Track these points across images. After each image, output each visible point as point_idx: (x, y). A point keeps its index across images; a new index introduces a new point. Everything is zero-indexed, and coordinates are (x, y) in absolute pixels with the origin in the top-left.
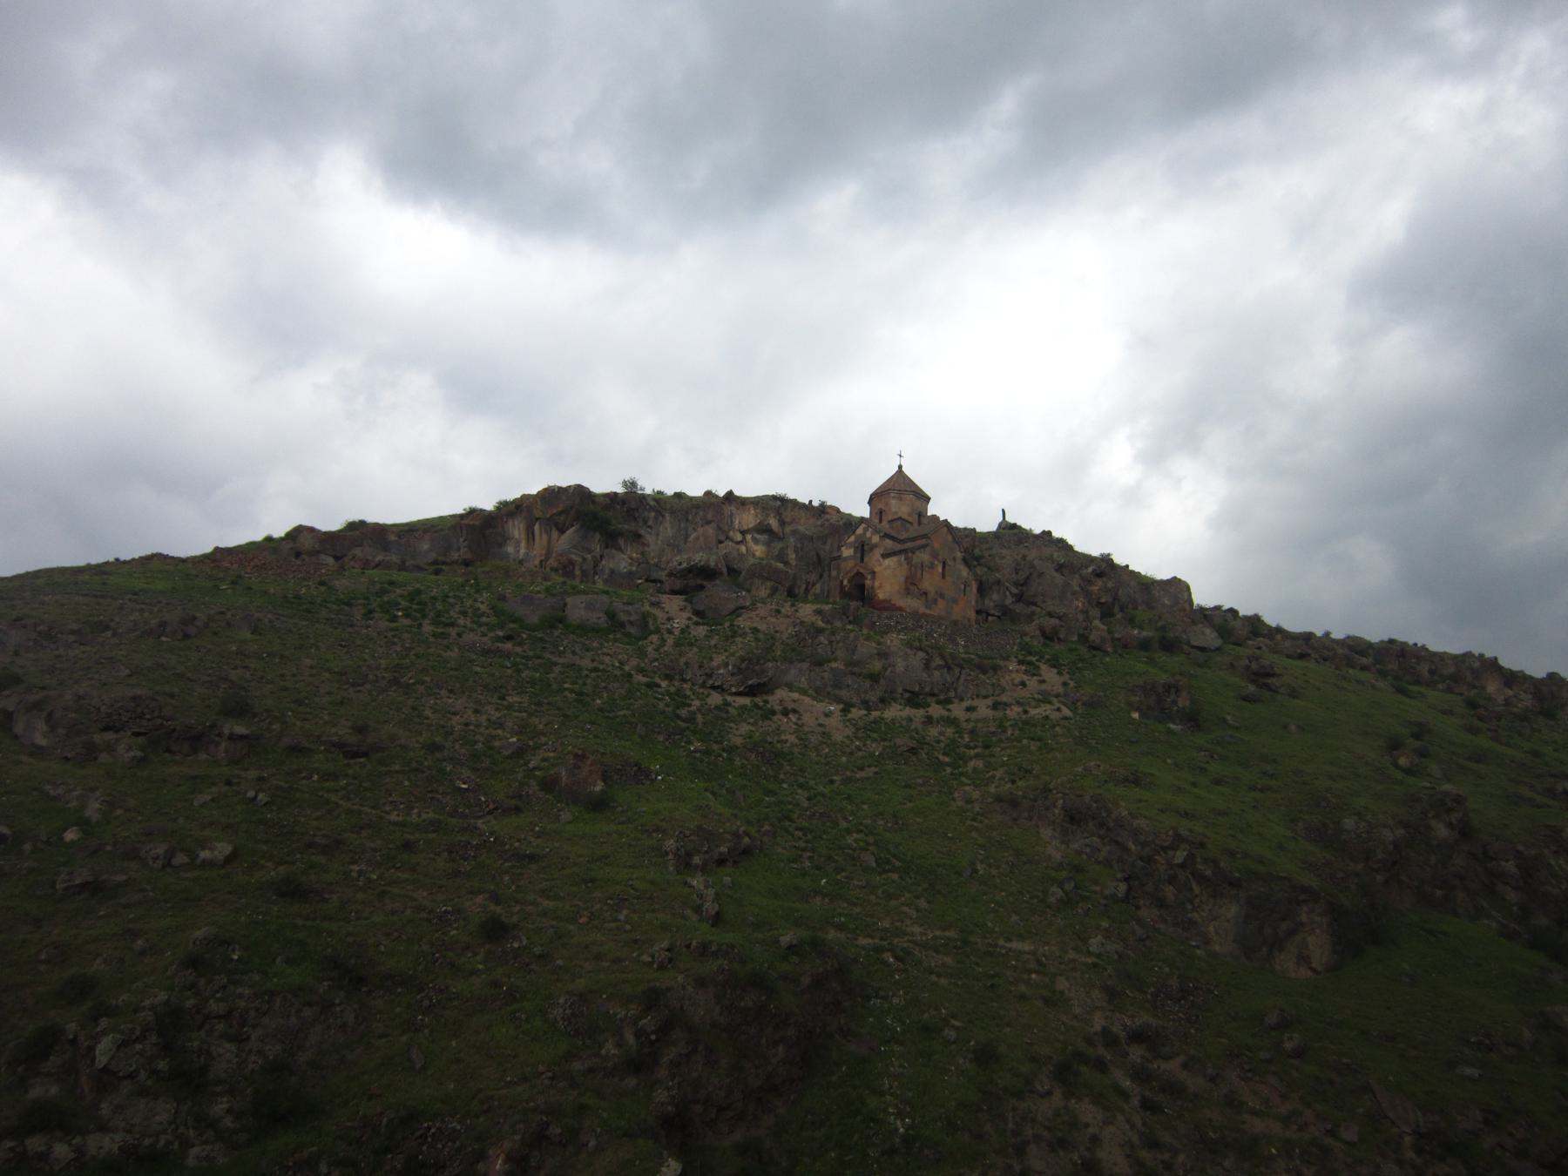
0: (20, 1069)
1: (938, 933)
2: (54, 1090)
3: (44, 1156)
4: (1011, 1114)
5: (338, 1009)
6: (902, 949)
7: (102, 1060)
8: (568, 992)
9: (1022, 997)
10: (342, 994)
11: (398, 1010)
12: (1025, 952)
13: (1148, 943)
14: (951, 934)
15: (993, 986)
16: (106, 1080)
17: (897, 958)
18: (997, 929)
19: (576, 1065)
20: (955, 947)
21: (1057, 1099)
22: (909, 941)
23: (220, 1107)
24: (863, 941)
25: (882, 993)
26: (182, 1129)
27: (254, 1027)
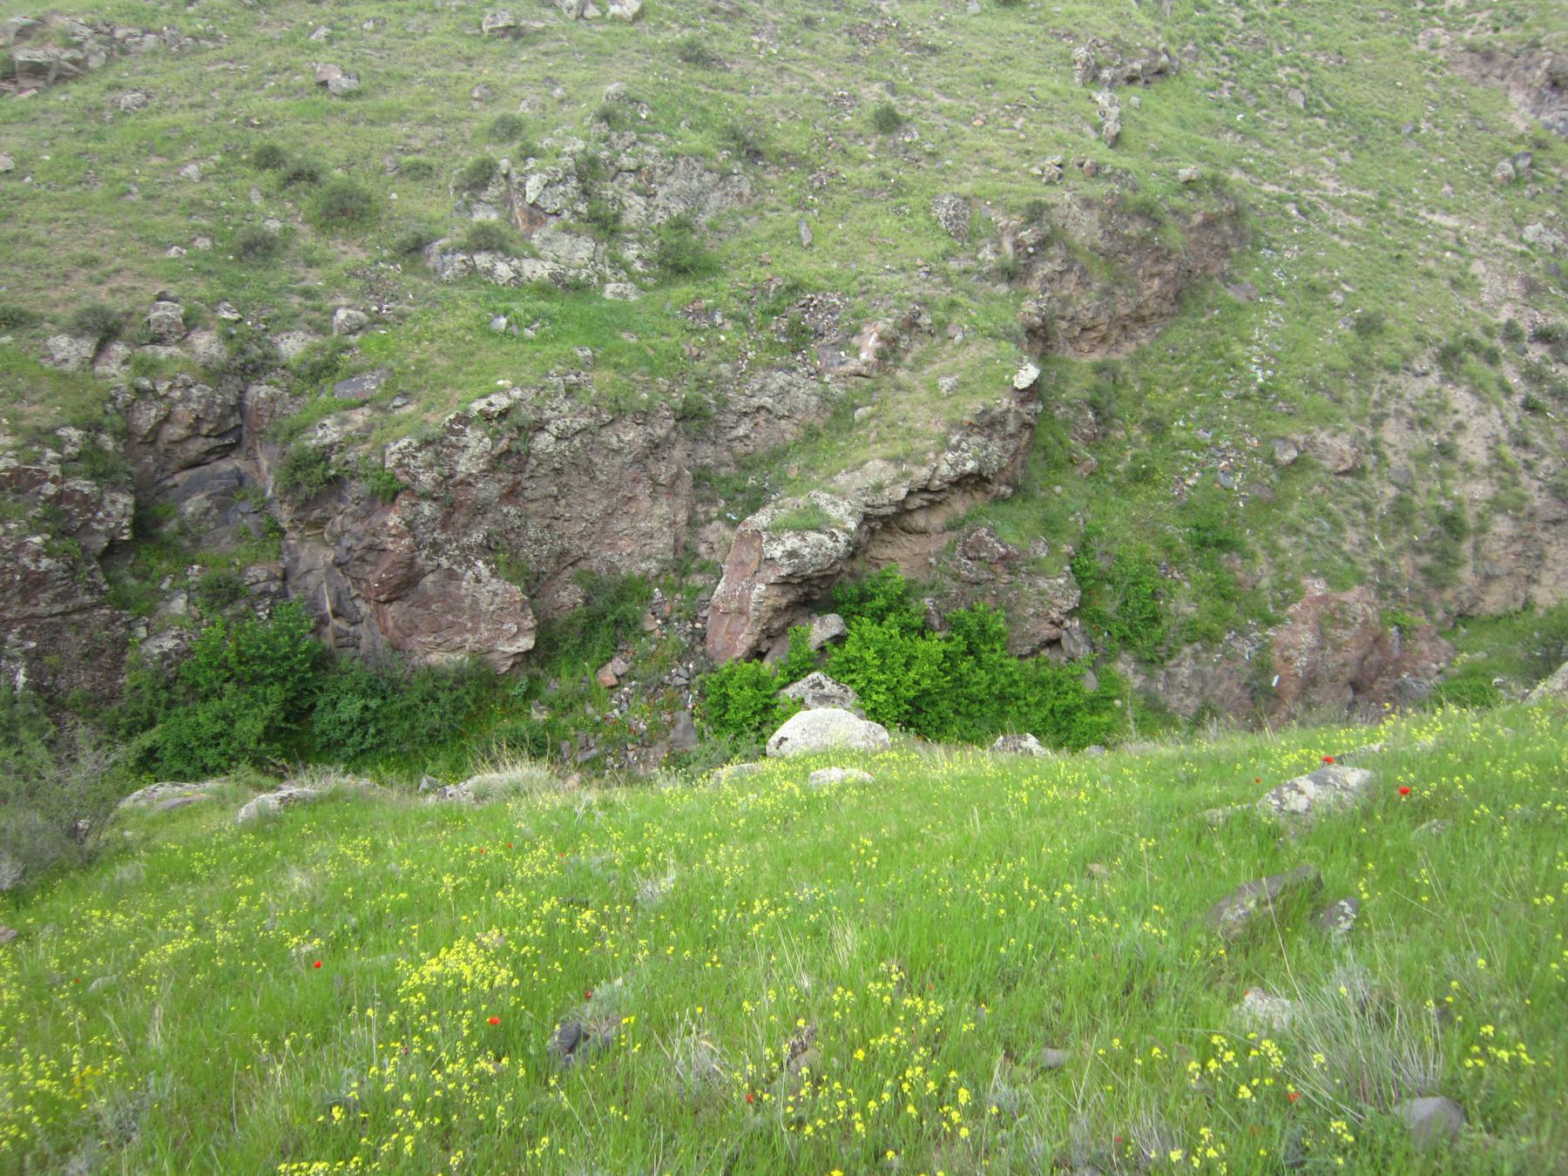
1: (1354, 192)
2: (494, 217)
3: (490, 272)
6: (1309, 203)
9: (1429, 275)
10: (739, 164)
12: (1446, 228)
14: (1369, 195)
15: (1398, 257)
16: (536, 215)
17: (1301, 211)
19: (953, 265)
20: (1369, 210)
21: (1432, 381)
23: (630, 253)
24: (1267, 188)
25: (1275, 245)
26: (600, 266)
27: (661, 184)
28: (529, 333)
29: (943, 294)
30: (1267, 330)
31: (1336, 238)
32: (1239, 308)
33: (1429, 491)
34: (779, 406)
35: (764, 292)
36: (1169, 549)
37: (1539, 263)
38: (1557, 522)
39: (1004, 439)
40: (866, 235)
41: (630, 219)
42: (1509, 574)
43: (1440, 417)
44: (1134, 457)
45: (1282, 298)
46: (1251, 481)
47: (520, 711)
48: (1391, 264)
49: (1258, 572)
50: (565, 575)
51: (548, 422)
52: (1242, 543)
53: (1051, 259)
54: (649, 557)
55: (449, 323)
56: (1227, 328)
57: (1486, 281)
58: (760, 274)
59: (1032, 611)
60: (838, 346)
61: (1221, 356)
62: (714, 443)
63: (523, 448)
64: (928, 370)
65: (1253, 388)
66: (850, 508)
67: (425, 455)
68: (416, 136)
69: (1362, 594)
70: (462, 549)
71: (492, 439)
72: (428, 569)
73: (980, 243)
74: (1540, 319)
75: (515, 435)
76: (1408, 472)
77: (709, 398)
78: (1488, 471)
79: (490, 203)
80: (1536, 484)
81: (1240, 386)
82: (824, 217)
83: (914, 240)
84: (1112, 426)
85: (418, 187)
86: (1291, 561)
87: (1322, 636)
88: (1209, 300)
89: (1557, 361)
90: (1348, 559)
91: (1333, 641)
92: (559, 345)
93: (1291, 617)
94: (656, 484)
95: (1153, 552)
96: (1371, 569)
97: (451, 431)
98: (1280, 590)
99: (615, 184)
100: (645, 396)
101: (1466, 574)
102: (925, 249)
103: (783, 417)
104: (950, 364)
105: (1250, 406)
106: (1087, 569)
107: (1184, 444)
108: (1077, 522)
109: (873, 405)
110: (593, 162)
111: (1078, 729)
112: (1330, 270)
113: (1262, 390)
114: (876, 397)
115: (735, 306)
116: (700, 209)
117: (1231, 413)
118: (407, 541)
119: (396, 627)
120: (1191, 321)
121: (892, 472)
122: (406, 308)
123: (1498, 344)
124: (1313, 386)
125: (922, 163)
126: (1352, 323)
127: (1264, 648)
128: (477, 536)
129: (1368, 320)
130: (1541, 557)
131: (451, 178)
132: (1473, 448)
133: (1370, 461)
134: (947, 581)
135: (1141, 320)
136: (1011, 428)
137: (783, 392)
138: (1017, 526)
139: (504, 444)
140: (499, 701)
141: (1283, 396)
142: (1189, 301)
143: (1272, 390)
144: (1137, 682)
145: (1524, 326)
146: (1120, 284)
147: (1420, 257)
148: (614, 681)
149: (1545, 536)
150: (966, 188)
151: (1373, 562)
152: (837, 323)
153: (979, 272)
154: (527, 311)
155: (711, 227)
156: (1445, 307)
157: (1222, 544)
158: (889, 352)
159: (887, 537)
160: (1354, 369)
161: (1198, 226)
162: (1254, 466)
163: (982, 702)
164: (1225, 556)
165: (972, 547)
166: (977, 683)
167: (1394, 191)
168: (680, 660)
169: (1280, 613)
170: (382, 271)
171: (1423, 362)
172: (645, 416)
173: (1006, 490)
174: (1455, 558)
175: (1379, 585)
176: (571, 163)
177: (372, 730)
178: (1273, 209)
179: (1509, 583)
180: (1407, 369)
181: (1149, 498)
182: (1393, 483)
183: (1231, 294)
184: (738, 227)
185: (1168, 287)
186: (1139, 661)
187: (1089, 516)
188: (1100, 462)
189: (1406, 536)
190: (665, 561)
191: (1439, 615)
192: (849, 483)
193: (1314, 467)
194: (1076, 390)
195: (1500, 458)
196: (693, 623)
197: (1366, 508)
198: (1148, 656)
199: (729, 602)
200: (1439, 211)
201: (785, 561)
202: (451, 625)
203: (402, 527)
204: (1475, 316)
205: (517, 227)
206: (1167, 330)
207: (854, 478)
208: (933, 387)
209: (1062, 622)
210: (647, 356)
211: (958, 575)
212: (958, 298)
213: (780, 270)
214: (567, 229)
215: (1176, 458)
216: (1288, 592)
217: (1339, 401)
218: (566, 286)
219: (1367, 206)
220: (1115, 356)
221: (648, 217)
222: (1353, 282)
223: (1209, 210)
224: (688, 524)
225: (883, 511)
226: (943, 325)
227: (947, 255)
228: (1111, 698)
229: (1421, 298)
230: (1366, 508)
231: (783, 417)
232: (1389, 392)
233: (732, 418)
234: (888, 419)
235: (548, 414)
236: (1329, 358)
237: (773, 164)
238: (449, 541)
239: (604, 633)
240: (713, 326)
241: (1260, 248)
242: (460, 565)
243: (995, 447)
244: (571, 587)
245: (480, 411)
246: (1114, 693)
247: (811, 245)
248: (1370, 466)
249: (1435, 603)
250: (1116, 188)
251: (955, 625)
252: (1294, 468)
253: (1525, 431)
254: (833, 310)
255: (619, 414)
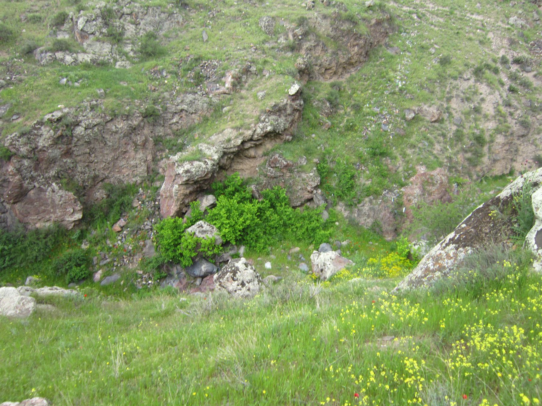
0: (54, 28)
1: (440, 8)
2: (67, 37)
3: (62, 60)
4: (449, 85)
5: (176, 15)
6: (422, 14)
7: (80, 26)
8: (268, 16)
9: (470, 39)
10: (178, 9)
11: (201, 18)
12: (478, 20)
13: (538, 22)
14: (447, 9)
15: (458, 33)
16: (84, 35)
17: (418, 17)
18: (468, 9)
19: (267, 45)
20: (446, 15)
21: (472, 82)
22: (426, 10)
23: (128, 49)
24: (405, 8)
25: (407, 31)
26: (114, 55)
27: (142, 19)
28: (76, 84)
29: (261, 58)
30: (404, 65)
31: (432, 27)
32: (392, 57)
33: (470, 127)
34: (190, 109)
35: (185, 62)
36: (360, 157)
37: (515, 32)
38: (523, 136)
39: (286, 116)
40: (230, 36)
41: (128, 34)
42: (503, 159)
43: (475, 96)
44: (347, 121)
45: (410, 52)
46: (395, 127)
47: (76, 245)
48: (455, 36)
49: (398, 165)
50: (98, 186)
51: (81, 122)
52: (391, 153)
53: (309, 41)
54: (136, 176)
55: (41, 82)
56: (387, 66)
57: (494, 41)
58: (184, 54)
59: (300, 187)
60: (216, 82)
61: (384, 77)
62: (163, 126)
63: (69, 133)
64: (254, 90)
65: (397, 89)
66: (216, 150)
67: (23, 140)
68: (36, 5)
69: (440, 171)
70: (46, 179)
71: (54, 131)
72: (30, 188)
73: (279, 36)
74: (515, 55)
75: (65, 128)
76: (461, 120)
77: (159, 107)
78: (494, 117)
79: (65, 31)
80: (514, 121)
81: (392, 89)
82: (214, 29)
83: (251, 37)
84: (338, 109)
85: (35, 26)
86: (412, 159)
87: (424, 190)
88: (380, 55)
89: (522, 71)
90: (436, 157)
91: (428, 191)
92: (89, 89)
93: (412, 183)
94: (136, 145)
95: (354, 159)
96: (445, 160)
97: (35, 128)
98: (407, 171)
99: (122, 20)
100: (128, 108)
101: (485, 160)
102: (254, 40)
103: (192, 113)
104: (263, 86)
105: (395, 96)
106: (324, 168)
107: (368, 114)
108: (321, 148)
109: (230, 105)
110: (110, 11)
111: (318, 237)
112: (430, 40)
113: (401, 90)
114: (232, 102)
115: (172, 68)
116: (160, 29)
117: (388, 100)
118: (18, 177)
119: (20, 213)
120: (373, 64)
121: (235, 133)
122: (23, 77)
123: (500, 67)
124: (422, 87)
125: (257, 5)
126: (438, 60)
127: (400, 196)
128: (52, 173)
129: (445, 59)
130: (517, 151)
131: (48, 22)
132: (488, 108)
133: (446, 116)
134: (262, 177)
135: (351, 64)
136: (289, 111)
137: (191, 103)
138: (292, 152)
139: (59, 133)
140: (67, 242)
141: (409, 92)
142: (372, 56)
143: (405, 90)
144: (346, 214)
145: (509, 58)
146: (340, 50)
147: (467, 33)
148: (119, 229)
149: (518, 142)
150: (274, 14)
151: (447, 157)
152: (215, 72)
153: (279, 48)
154: (76, 75)
155: (166, 36)
156: (477, 52)
157: (382, 154)
158: (238, 82)
159: (240, 160)
160: (439, 79)
161: (374, 25)
162: (397, 121)
163: (276, 228)
164: (384, 159)
165: (272, 163)
166: (274, 220)
167: (457, 7)
168: (148, 218)
169: (407, 182)
170: (15, 62)
171: (467, 74)
172: (128, 117)
173: (289, 138)
174: (481, 154)
175: (449, 167)
176: (98, 11)
177: (7, 259)
178: (407, 17)
179: (503, 162)
180: (461, 78)
181: (352, 137)
182: (455, 124)
183: (390, 52)
184: (177, 35)
185: (361, 50)
186: (346, 205)
187: (327, 146)
188: (333, 124)
189: (460, 146)
190: (143, 177)
191: (475, 177)
192: (216, 140)
193: (422, 120)
194: (323, 94)
195: (499, 111)
196: (155, 202)
197: (444, 136)
198: (349, 203)
199: (166, 193)
200: (475, 14)
201: (184, 174)
202: (44, 211)
203: (15, 171)
204: (489, 55)
205: (77, 40)
206: (363, 68)
207: (218, 137)
208: (256, 97)
209: (312, 191)
210: (131, 91)
211: (267, 175)
212: (268, 59)
213: (193, 52)
214: (98, 40)
215: (365, 120)
216: (410, 172)
217: (433, 92)
218: (98, 64)
219: (445, 13)
220: (341, 80)
221: (136, 33)
222: (439, 44)
223: (378, 18)
224: (153, 161)
225: (232, 150)
226: (261, 71)
227: (264, 42)
228: (334, 222)
229: (467, 49)
230: (444, 136)
231: (192, 113)
232: (453, 88)
233: (169, 116)
234: (236, 111)
235: (81, 118)
236: (429, 75)
237: (193, 8)
238: (39, 176)
239: (116, 209)
240: (162, 77)
241: (401, 33)
242: (45, 185)
243: (282, 120)
244: (101, 191)
245: (49, 119)
246: (334, 220)
247: (207, 41)
248: (445, 118)
249: (473, 173)
250: (337, 10)
251: (266, 196)
252: (414, 121)
253: (509, 100)
254: (214, 67)
255: (115, 116)
